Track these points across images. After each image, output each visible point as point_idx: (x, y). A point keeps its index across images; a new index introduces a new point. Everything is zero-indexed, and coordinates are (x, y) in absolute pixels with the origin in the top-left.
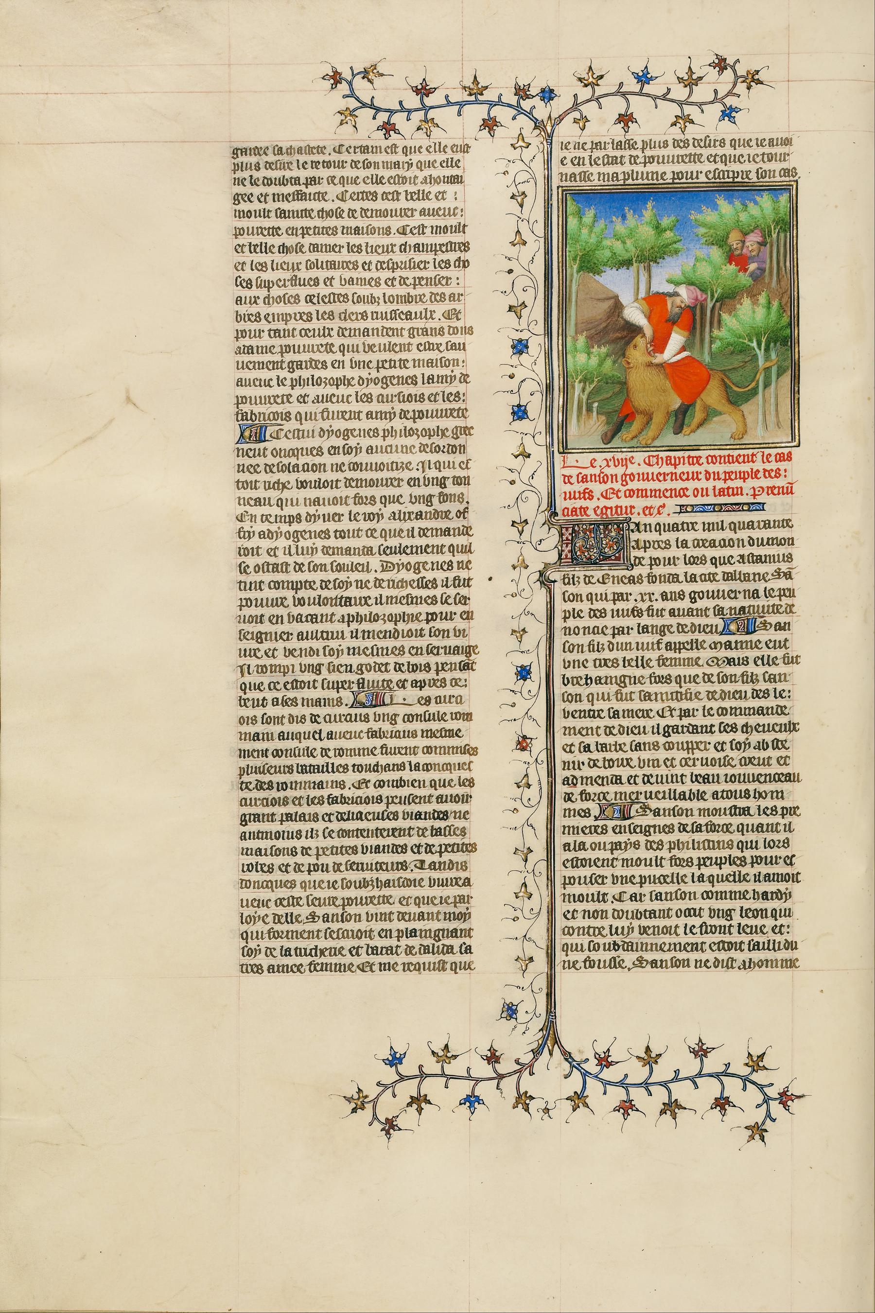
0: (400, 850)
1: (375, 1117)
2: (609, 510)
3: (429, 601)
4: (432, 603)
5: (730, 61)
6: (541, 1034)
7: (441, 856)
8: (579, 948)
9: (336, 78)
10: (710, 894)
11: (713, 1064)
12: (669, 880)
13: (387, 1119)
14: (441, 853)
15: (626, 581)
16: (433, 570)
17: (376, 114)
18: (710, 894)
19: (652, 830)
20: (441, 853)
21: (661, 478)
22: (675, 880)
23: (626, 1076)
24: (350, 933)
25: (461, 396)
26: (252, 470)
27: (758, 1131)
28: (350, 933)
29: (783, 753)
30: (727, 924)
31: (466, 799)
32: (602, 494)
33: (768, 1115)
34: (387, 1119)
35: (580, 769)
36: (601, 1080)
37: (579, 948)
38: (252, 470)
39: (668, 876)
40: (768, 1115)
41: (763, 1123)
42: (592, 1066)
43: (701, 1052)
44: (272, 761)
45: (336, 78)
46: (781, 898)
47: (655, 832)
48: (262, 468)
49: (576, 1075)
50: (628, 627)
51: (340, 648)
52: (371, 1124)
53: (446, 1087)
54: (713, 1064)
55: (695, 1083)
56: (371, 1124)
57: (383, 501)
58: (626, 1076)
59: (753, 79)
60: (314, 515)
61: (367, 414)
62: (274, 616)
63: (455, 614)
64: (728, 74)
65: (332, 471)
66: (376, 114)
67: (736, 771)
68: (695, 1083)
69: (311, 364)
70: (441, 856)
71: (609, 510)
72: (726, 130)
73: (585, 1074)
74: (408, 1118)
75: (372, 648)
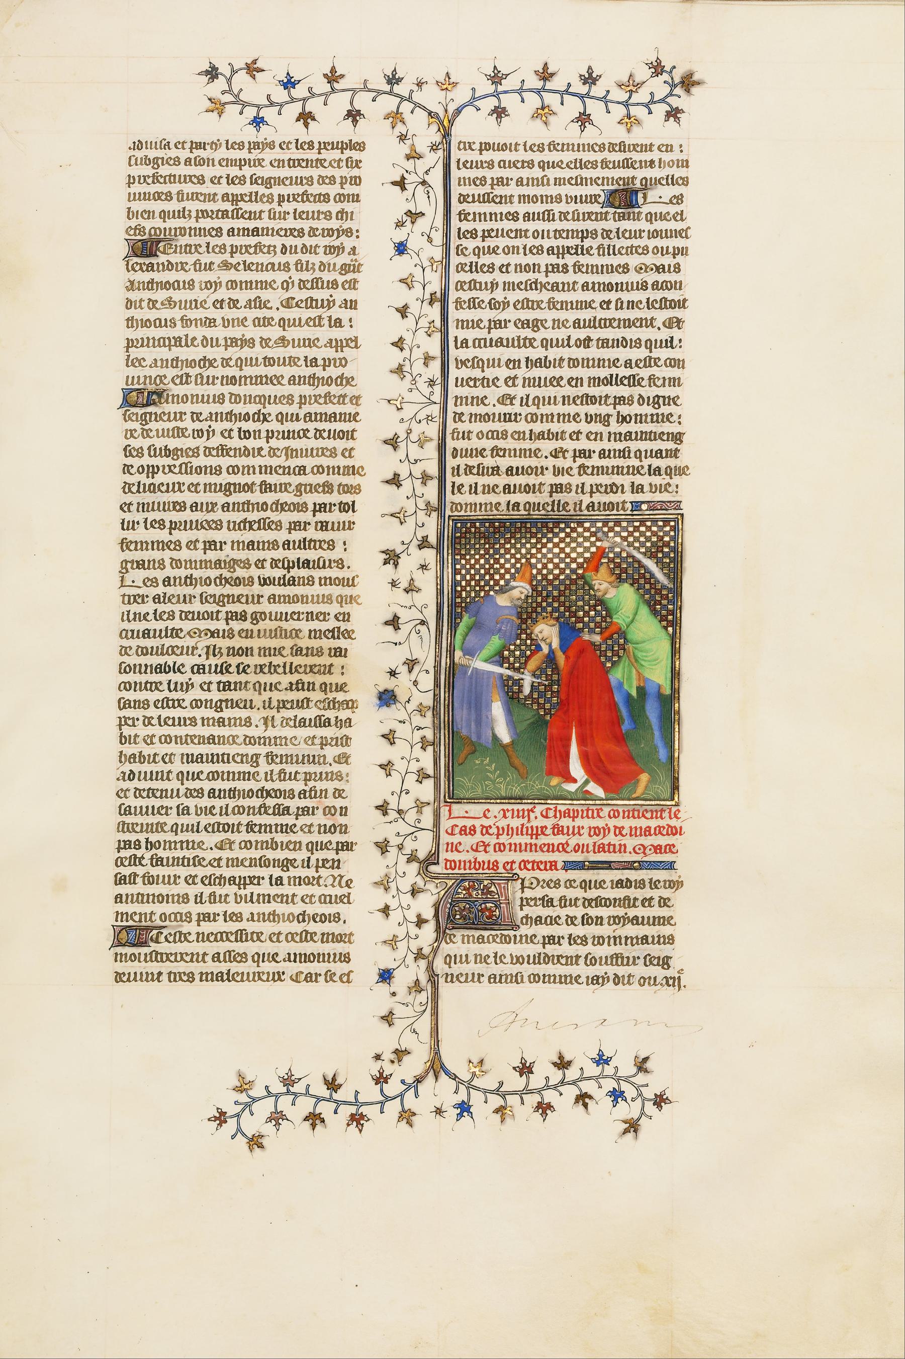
0: (163, 197)
1: (239, 1130)
3: (214, 233)
4: (216, 235)
5: (667, 68)
8: (297, 323)
10: (199, 703)
18: (199, 703)
19: (224, 704)
21: (472, 383)
22: (578, 165)
25: (354, 232)
30: (252, 770)
32: (498, 401)
37: (297, 323)
44: (336, 480)
47: (227, 708)
50: (590, 451)
51: (331, 299)
52: (233, 1137)
54: (394, 1108)
56: (233, 1137)
57: (257, 688)
59: (688, 83)
61: (490, 978)
65: (289, 885)
67: (328, 769)
69: (138, 898)
72: (669, 132)
74: (642, 74)
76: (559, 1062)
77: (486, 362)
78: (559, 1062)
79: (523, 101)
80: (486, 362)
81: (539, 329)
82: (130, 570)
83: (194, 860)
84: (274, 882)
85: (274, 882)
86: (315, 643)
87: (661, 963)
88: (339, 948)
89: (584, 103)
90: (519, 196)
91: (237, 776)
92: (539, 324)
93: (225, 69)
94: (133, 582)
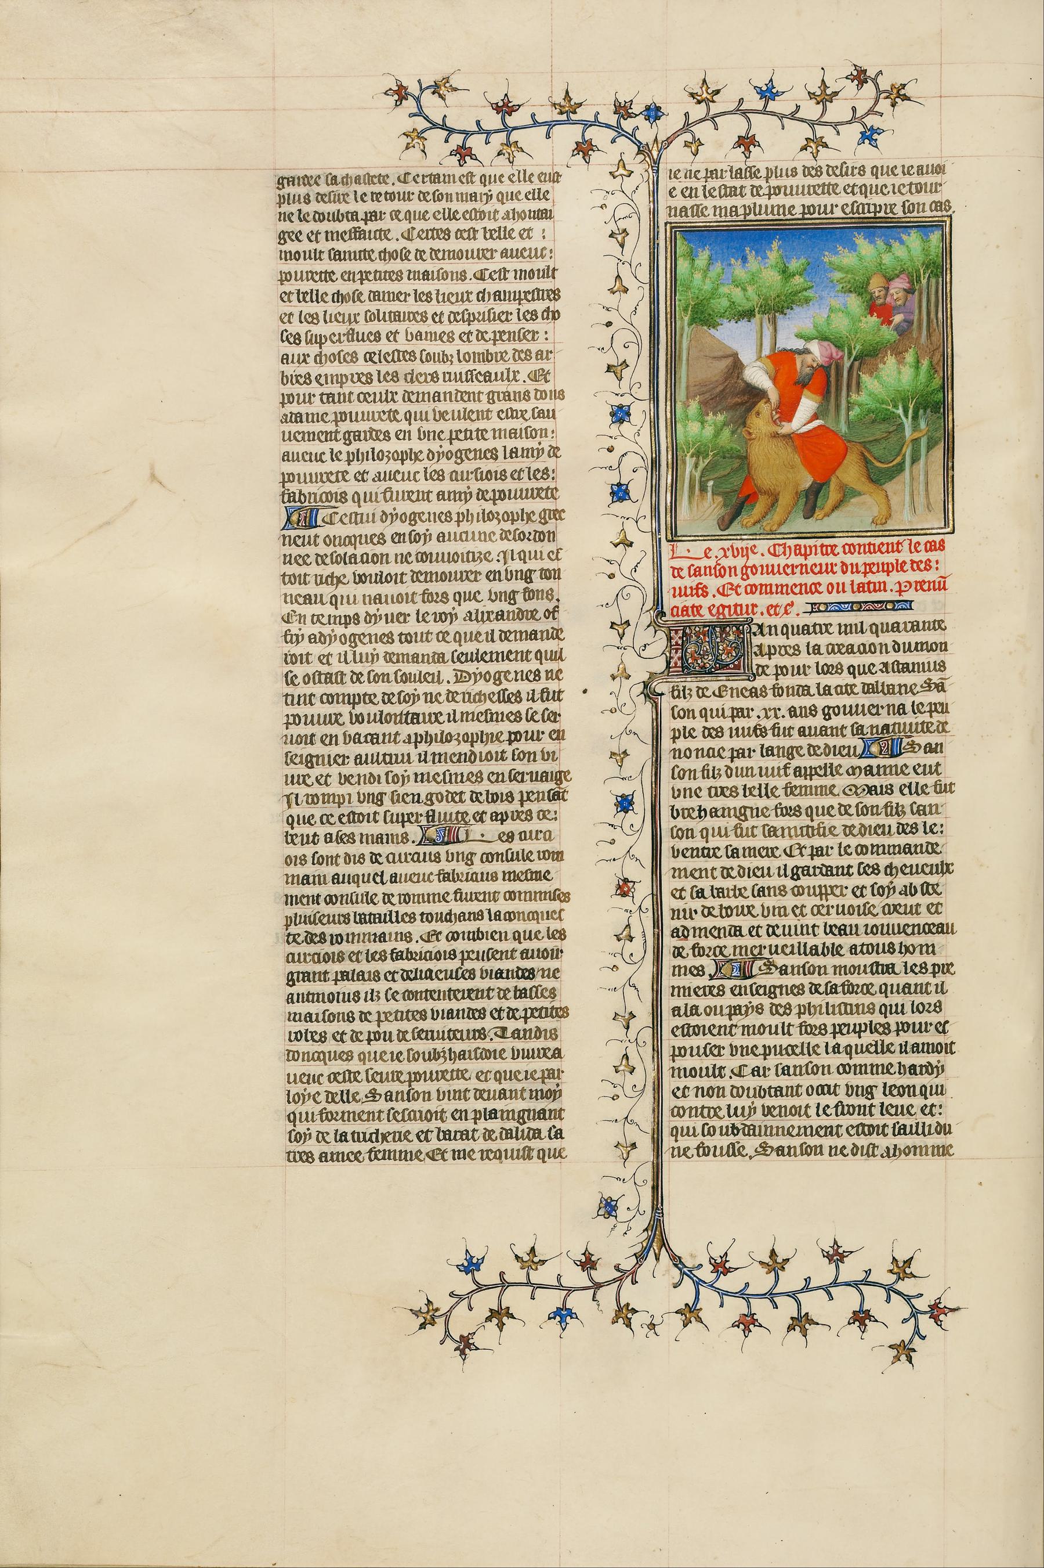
2: (727, 610)
3: (512, 718)
5: (871, 73)
6: (645, 1234)
7: (526, 1023)
8: (691, 1133)
9: (401, 93)
10: (847, 1068)
11: (851, 1270)
12: (798, 1051)
13: (462, 1337)
14: (526, 1018)
15: (747, 694)
16: (516, 680)
17: (448, 136)
18: (847, 1068)
20: (526, 1018)
23: (747, 1285)
24: (418, 1115)
26: (300, 561)
27: (904, 1351)
28: (418, 1115)
29: (934, 899)
30: (868, 1103)
31: (556, 954)
33: (917, 1332)
34: (462, 1337)
35: (692, 919)
36: (717, 1290)
37: (691, 1133)
38: (300, 561)
39: (797, 1046)
40: (917, 1332)
41: (911, 1341)
42: (706, 1274)
43: (836, 1256)
45: (401, 93)
46: (932, 1073)
48: (312, 559)
49: (688, 1284)
53: (533, 1298)
54: (851, 1270)
55: (829, 1293)
58: (747, 1285)
59: (898, 94)
60: (375, 615)
62: (326, 736)
63: (543, 733)
64: (869, 88)
66: (448, 136)
68: (829, 1293)
70: (526, 1023)
71: (727, 610)
73: (698, 1283)
75: (444, 774)
76: (505, 1320)
77: (463, 636)
78: (505, 1320)
79: (838, 133)
80: (463, 636)
81: (285, 242)
82: (749, 817)
83: (705, 1048)
84: (811, 650)
85: (811, 650)
86: (490, 868)
87: (516, 1117)
88: (934, 657)
89: (749, 1303)
90: (327, 232)
91: (774, 1131)
92: (286, 236)
93: (414, 89)
94: (483, 835)
